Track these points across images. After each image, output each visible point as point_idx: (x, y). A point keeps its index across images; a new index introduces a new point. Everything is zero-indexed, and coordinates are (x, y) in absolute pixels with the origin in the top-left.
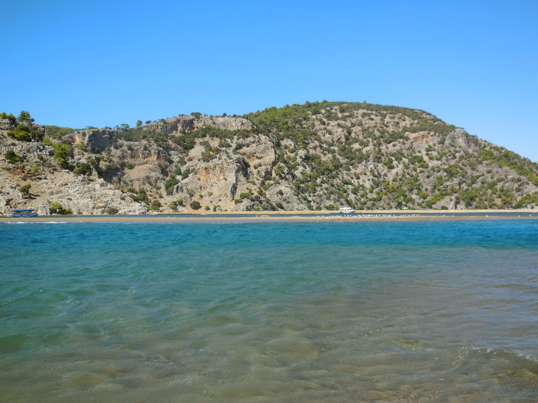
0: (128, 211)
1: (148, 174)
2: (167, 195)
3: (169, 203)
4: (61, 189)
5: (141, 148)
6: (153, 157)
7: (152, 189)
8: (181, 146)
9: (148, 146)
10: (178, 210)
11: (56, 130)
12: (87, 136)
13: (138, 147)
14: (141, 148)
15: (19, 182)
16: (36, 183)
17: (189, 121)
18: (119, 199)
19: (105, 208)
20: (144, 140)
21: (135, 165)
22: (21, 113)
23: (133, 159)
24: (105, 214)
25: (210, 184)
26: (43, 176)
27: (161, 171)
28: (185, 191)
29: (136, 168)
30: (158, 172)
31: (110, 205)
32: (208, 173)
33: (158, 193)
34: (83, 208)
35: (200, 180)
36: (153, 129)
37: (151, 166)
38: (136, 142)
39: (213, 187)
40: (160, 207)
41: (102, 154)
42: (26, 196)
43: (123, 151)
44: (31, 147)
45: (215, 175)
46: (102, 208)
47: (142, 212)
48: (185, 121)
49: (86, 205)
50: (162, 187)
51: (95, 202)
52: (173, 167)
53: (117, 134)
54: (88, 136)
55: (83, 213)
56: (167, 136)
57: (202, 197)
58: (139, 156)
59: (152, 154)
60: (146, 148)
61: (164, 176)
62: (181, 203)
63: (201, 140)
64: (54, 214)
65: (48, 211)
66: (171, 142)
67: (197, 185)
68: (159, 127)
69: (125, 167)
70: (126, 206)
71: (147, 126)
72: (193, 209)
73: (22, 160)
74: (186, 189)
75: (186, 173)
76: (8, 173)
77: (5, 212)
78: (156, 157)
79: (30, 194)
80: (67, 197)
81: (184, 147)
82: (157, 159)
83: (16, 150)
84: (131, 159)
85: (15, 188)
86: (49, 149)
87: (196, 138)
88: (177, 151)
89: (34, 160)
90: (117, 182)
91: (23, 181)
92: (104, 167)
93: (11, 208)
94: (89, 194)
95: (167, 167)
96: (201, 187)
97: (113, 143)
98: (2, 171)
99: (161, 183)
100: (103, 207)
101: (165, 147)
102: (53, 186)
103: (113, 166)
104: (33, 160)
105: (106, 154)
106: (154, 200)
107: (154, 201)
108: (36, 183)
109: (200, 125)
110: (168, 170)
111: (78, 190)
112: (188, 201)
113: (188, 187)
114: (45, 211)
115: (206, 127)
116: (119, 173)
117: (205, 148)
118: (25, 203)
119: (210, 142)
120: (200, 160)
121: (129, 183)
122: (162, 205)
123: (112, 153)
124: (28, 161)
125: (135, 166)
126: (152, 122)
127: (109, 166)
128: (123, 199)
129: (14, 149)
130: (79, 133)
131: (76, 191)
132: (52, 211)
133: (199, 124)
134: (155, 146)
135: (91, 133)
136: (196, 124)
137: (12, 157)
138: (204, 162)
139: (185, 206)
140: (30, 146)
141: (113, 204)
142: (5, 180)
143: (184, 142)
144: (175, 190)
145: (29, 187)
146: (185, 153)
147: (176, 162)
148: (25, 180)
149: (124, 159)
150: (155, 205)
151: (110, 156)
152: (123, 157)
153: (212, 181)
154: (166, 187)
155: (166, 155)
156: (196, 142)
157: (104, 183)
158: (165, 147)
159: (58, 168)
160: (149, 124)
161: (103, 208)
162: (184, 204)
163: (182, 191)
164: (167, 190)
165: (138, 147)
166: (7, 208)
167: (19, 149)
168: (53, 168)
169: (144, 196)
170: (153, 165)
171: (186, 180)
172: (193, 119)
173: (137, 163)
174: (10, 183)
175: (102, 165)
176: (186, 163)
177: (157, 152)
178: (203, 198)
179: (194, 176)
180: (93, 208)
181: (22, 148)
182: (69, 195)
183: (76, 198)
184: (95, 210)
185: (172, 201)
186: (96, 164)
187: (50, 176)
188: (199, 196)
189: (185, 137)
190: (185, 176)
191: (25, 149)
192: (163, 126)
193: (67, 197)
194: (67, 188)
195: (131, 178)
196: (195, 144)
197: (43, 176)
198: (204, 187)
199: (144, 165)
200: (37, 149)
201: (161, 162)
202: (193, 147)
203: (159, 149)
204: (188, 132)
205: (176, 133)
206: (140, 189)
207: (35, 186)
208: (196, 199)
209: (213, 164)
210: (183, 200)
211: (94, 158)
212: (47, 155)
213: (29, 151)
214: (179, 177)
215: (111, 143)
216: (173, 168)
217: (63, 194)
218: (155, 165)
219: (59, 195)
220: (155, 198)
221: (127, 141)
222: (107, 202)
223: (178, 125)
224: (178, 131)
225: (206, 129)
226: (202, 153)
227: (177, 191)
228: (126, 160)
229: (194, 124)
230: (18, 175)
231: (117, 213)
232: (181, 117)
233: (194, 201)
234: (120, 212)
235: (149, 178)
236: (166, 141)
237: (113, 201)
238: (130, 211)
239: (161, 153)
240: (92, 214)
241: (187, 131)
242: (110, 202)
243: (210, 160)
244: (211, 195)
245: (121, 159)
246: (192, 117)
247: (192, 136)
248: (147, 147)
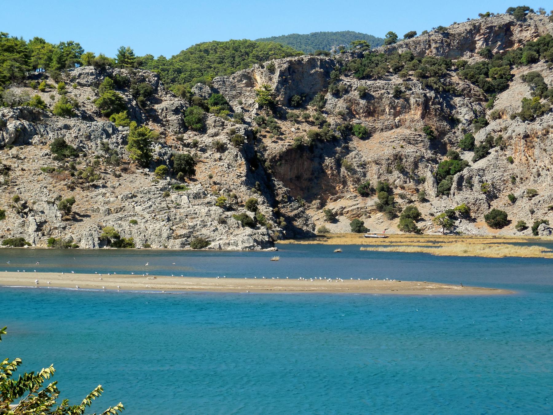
0: (224, 244)
1: (399, 149)
2: (437, 196)
3: (439, 214)
4: (124, 204)
5: (389, 93)
6: (413, 112)
7: (406, 182)
8: (478, 86)
9: (403, 89)
10: (458, 230)
11: (247, 50)
12: (277, 73)
13: (383, 91)
14: (389, 93)
15: (63, 192)
16: (89, 194)
17: (500, 28)
18: (215, 223)
19: (189, 237)
20: (397, 76)
21: (374, 130)
22: (119, 51)
23: (371, 118)
24: (188, 248)
25: (535, 170)
26: (100, 183)
27: (430, 142)
28: (477, 186)
29: (376, 135)
30: (422, 144)
31: (198, 233)
32: (530, 146)
33: (417, 190)
34: (152, 236)
35: (512, 162)
36: (418, 50)
37: (407, 132)
38: (378, 81)
39: (541, 178)
40: (417, 221)
41: (307, 109)
42: (68, 217)
43: (350, 100)
44: (93, 131)
45: (545, 150)
46: (184, 237)
47: (248, 245)
48: (491, 28)
49: (158, 233)
50: (427, 178)
51: (174, 228)
52: (458, 133)
53: (341, 64)
54: (278, 73)
55: (151, 246)
56: (448, 67)
57: (513, 200)
58: (384, 111)
59: (412, 107)
60: (398, 94)
61: (436, 153)
62: (466, 214)
63: (525, 70)
64: (105, 247)
65: (97, 242)
66: (456, 77)
67: (505, 174)
68: (433, 45)
69: (354, 134)
70: (226, 235)
71: (407, 45)
72: (491, 226)
73: (75, 153)
74: (480, 182)
75: (484, 147)
76: (49, 178)
77: (34, 242)
78: (419, 113)
79: (75, 213)
80: (130, 219)
81: (485, 88)
82: (423, 116)
83: (69, 138)
84: (365, 117)
85: (54, 203)
86: (124, 133)
87: (514, 66)
88: (468, 96)
89: (96, 154)
90: (332, 168)
91: (69, 190)
92: (306, 138)
93: (43, 235)
94: (165, 213)
95: (443, 133)
96: (514, 179)
97: (330, 86)
98: (41, 173)
99: (425, 170)
100: (184, 236)
101: (441, 89)
102: (112, 199)
103: (326, 134)
104: (94, 153)
105: (315, 108)
106: (408, 205)
107: (407, 208)
108: (89, 194)
109: (527, 35)
110: (446, 139)
111: (151, 206)
112: (481, 208)
113: (484, 178)
114: (91, 242)
115: (539, 40)
116: (338, 149)
117: (532, 88)
118: (64, 228)
119: (544, 74)
120: (515, 117)
121: (358, 170)
122: (423, 216)
123: (328, 107)
124: (85, 155)
125: (375, 132)
126: (419, 33)
127: (317, 134)
128: (223, 222)
129: (67, 134)
130: (263, 67)
131: (146, 208)
132: (104, 241)
133: (524, 34)
134: (418, 90)
135: (285, 66)
136: (517, 34)
137: (61, 150)
138: (524, 121)
139: (474, 220)
140: (92, 129)
141: (204, 231)
142: (42, 190)
143: (487, 75)
144: (454, 185)
145: (72, 201)
146: (487, 100)
147: (464, 122)
148: (73, 189)
149: (351, 118)
150: (408, 217)
151: (323, 112)
152: (350, 114)
153: (539, 164)
154: (435, 177)
155: (442, 108)
156: (513, 75)
157: (200, 194)
158: (441, 89)
159: (132, 167)
160: (412, 39)
161: (185, 238)
162: (473, 215)
163: (471, 186)
164: (438, 184)
165: (383, 91)
166: (38, 235)
167: (74, 135)
168: (123, 166)
169: (388, 198)
170: (413, 129)
171: (482, 163)
172: (511, 24)
173: (379, 125)
174: (48, 194)
175: (304, 133)
176: (487, 124)
177: (421, 100)
178: (517, 203)
179: (501, 153)
180: (168, 237)
181: (78, 133)
182: (134, 216)
183: (144, 221)
184: (172, 241)
185: (447, 209)
186: (244, 143)
187: (112, 181)
188: (507, 198)
189: (490, 65)
190: (483, 153)
191: (83, 134)
192: (442, 42)
193: (130, 219)
194: (133, 203)
195: (362, 159)
196: (512, 81)
197: (100, 183)
198: (522, 179)
199: (393, 130)
200: (102, 134)
201: (430, 123)
202: (505, 87)
203: (428, 95)
204: (497, 53)
205: (470, 57)
206: (380, 183)
207: (85, 200)
208: (498, 205)
209: (541, 127)
210: (472, 207)
211: (242, 132)
212: (117, 143)
213: (89, 138)
214: (468, 156)
215: (326, 87)
216: (458, 135)
217: (126, 213)
218: (416, 130)
219: (119, 215)
220: (411, 202)
221: (360, 79)
222: (194, 227)
223: (476, 39)
224: (476, 51)
225: (538, 45)
226: (525, 100)
227: (460, 187)
228: (355, 121)
229: (512, 35)
230: (64, 180)
231: (206, 246)
232: (484, 19)
233: (494, 210)
234: (212, 245)
235: (401, 159)
236: (444, 76)
237: (205, 226)
238: (229, 244)
239: (430, 103)
240: (166, 247)
241: (495, 51)
242: (198, 227)
243: (538, 116)
244: (533, 196)
245: (345, 119)
246: (508, 19)
247: (505, 61)
248: (401, 92)
